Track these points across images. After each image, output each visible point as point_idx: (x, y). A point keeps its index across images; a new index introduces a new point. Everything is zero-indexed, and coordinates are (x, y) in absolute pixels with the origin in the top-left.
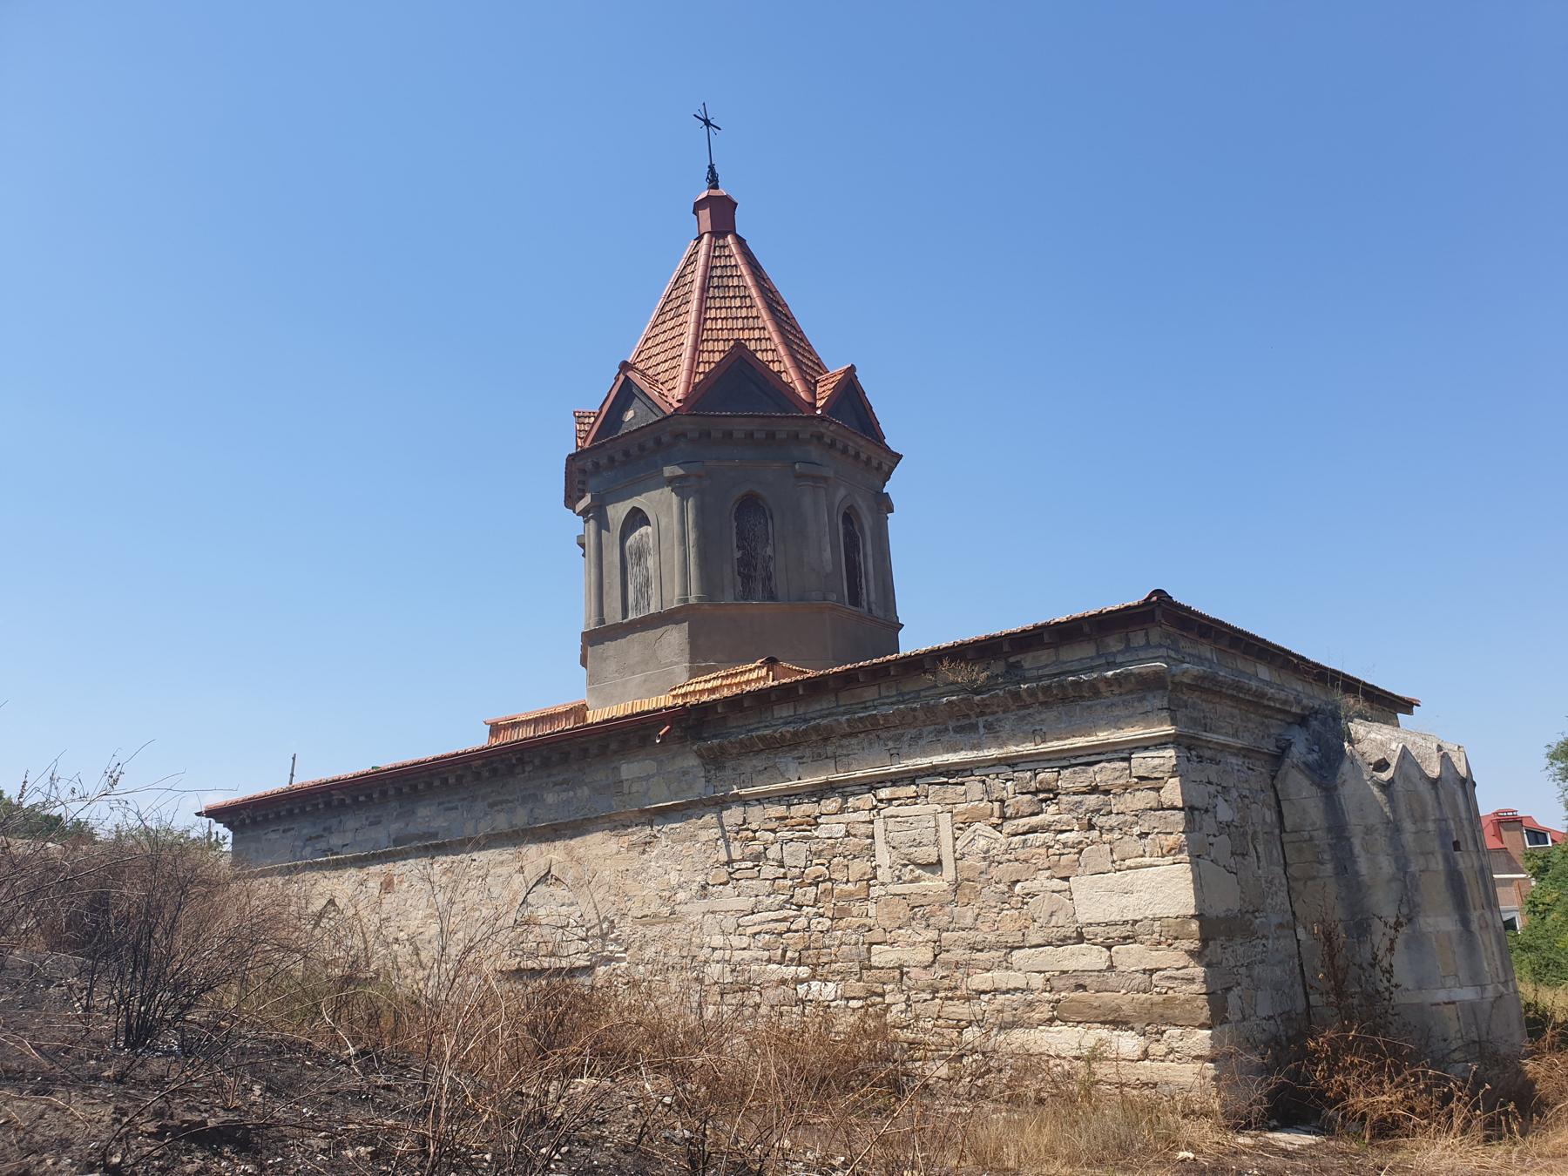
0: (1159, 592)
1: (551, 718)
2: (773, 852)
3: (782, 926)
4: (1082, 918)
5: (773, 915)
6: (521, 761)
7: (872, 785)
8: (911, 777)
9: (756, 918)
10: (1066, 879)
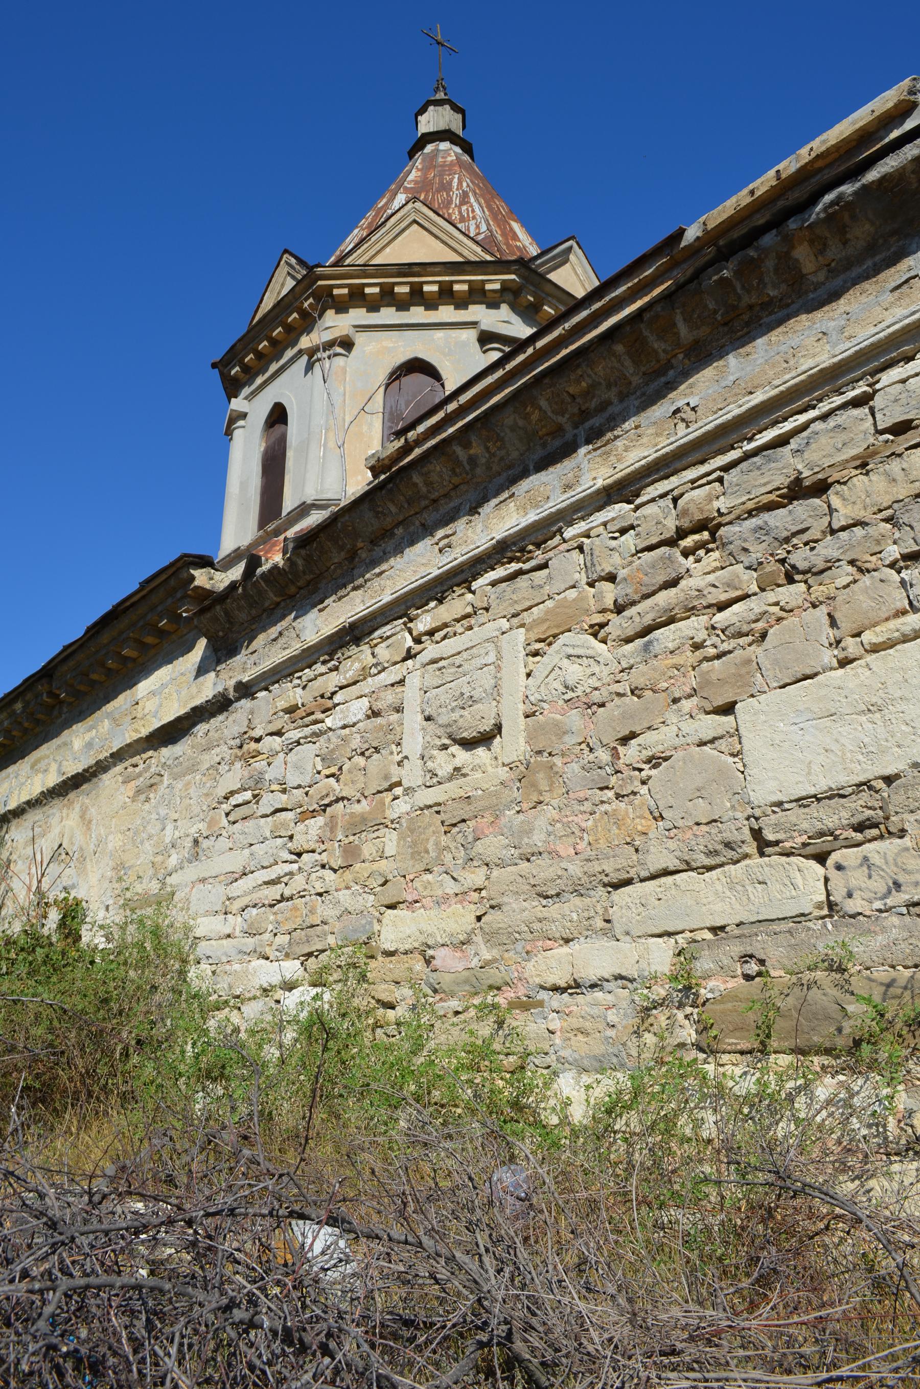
3: (274, 892)
4: (763, 792)
10: (728, 709)
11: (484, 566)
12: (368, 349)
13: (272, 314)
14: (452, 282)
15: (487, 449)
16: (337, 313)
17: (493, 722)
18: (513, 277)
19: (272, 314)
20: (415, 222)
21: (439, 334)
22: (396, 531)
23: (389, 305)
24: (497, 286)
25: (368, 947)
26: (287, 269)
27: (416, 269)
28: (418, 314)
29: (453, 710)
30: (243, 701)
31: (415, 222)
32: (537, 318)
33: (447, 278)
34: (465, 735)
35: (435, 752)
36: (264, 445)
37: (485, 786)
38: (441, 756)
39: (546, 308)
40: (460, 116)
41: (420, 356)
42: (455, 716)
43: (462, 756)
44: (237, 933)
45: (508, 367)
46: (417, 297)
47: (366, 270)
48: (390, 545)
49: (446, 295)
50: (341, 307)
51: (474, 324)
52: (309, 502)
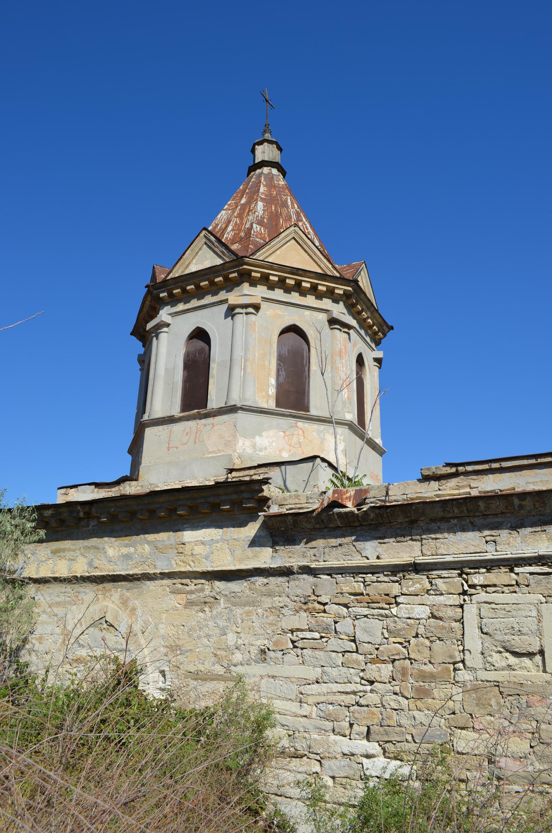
0: (198, 328)
1: (488, 492)
2: (345, 626)
3: (350, 699)
5: (341, 687)
6: (88, 516)
7: (462, 567)
8: (511, 564)
9: (324, 688)
11: (524, 563)
12: (268, 313)
13: (203, 272)
14: (318, 284)
15: (534, 505)
16: (250, 286)
17: (538, 648)
18: (350, 289)
19: (203, 272)
20: (294, 238)
21: (307, 312)
22: (452, 520)
23: (280, 288)
24: (341, 292)
25: (447, 748)
26: (204, 240)
27: (300, 272)
28: (295, 297)
29: (505, 634)
30: (305, 576)
31: (294, 238)
32: (352, 310)
33: (316, 281)
34: (516, 650)
35: (494, 654)
36: (185, 349)
37: (533, 680)
38: (496, 656)
39: (358, 306)
40: (266, 144)
41: (297, 324)
42: (507, 638)
43: (512, 660)
44: (314, 716)
45: (539, 460)
46: (297, 287)
47: (273, 266)
48: (444, 525)
49: (313, 290)
50: (253, 283)
51: (326, 311)
52: (239, 406)
